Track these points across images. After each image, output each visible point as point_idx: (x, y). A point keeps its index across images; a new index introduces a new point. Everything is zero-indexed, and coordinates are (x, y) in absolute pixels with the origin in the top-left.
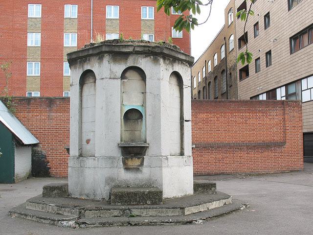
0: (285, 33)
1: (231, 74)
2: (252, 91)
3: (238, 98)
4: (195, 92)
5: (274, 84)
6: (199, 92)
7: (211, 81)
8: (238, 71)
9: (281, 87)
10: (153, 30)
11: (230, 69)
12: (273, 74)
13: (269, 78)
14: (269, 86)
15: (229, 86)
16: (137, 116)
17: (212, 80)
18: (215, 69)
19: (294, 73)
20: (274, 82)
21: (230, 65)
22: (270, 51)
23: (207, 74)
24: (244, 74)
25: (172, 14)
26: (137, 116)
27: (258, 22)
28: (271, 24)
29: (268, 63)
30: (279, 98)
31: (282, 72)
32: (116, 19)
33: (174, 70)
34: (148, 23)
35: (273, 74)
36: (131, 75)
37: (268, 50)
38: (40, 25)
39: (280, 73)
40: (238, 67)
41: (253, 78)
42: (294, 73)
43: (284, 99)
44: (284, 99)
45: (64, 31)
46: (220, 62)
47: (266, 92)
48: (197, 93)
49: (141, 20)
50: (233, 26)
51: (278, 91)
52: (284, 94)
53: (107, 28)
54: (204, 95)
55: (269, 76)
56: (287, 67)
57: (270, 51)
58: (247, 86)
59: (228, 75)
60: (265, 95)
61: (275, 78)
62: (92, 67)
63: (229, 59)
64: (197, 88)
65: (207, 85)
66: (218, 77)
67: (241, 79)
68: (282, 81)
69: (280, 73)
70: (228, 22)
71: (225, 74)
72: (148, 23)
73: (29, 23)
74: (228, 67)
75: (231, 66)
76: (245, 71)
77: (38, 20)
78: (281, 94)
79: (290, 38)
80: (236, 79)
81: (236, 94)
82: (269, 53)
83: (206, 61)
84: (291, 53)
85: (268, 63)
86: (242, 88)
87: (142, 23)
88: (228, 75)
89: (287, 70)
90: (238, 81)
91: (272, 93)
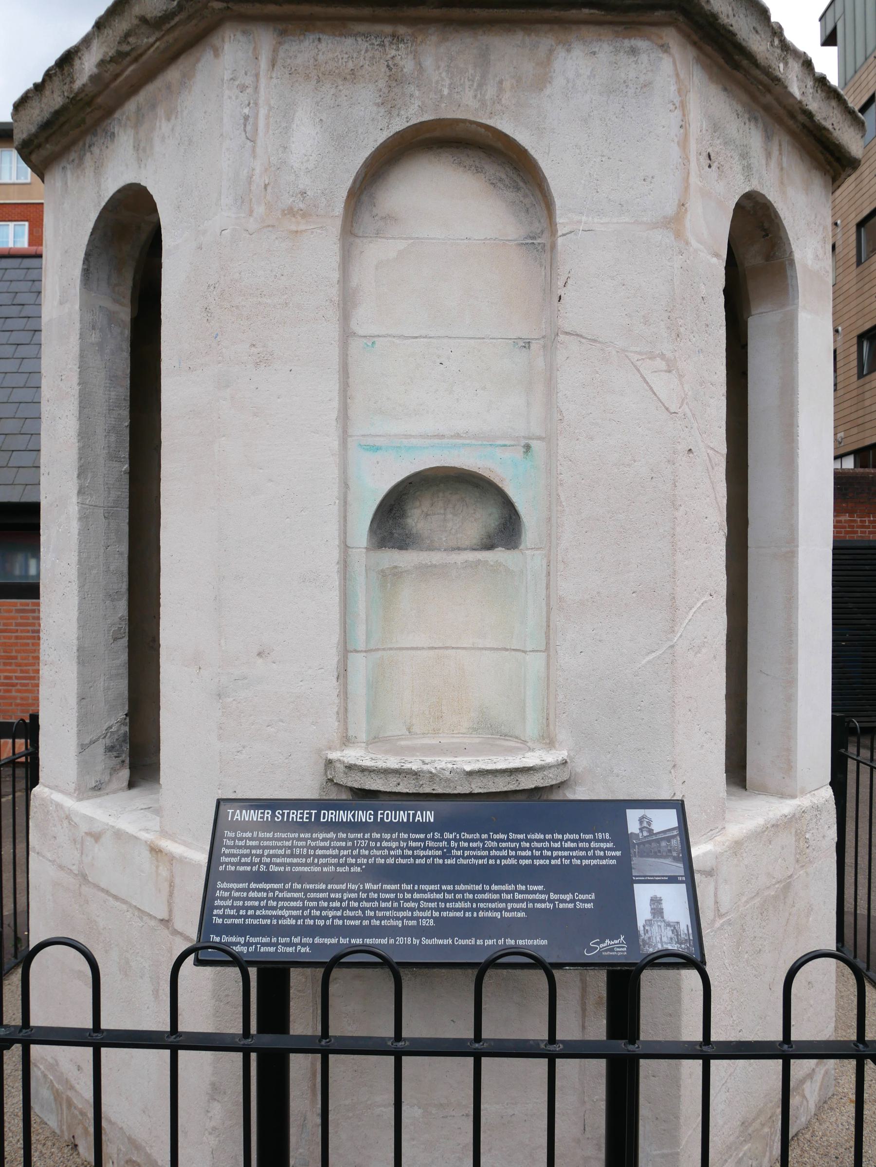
14: (868, 433)
16: (478, 520)
26: (478, 520)
55: (867, 403)
62: (141, 150)
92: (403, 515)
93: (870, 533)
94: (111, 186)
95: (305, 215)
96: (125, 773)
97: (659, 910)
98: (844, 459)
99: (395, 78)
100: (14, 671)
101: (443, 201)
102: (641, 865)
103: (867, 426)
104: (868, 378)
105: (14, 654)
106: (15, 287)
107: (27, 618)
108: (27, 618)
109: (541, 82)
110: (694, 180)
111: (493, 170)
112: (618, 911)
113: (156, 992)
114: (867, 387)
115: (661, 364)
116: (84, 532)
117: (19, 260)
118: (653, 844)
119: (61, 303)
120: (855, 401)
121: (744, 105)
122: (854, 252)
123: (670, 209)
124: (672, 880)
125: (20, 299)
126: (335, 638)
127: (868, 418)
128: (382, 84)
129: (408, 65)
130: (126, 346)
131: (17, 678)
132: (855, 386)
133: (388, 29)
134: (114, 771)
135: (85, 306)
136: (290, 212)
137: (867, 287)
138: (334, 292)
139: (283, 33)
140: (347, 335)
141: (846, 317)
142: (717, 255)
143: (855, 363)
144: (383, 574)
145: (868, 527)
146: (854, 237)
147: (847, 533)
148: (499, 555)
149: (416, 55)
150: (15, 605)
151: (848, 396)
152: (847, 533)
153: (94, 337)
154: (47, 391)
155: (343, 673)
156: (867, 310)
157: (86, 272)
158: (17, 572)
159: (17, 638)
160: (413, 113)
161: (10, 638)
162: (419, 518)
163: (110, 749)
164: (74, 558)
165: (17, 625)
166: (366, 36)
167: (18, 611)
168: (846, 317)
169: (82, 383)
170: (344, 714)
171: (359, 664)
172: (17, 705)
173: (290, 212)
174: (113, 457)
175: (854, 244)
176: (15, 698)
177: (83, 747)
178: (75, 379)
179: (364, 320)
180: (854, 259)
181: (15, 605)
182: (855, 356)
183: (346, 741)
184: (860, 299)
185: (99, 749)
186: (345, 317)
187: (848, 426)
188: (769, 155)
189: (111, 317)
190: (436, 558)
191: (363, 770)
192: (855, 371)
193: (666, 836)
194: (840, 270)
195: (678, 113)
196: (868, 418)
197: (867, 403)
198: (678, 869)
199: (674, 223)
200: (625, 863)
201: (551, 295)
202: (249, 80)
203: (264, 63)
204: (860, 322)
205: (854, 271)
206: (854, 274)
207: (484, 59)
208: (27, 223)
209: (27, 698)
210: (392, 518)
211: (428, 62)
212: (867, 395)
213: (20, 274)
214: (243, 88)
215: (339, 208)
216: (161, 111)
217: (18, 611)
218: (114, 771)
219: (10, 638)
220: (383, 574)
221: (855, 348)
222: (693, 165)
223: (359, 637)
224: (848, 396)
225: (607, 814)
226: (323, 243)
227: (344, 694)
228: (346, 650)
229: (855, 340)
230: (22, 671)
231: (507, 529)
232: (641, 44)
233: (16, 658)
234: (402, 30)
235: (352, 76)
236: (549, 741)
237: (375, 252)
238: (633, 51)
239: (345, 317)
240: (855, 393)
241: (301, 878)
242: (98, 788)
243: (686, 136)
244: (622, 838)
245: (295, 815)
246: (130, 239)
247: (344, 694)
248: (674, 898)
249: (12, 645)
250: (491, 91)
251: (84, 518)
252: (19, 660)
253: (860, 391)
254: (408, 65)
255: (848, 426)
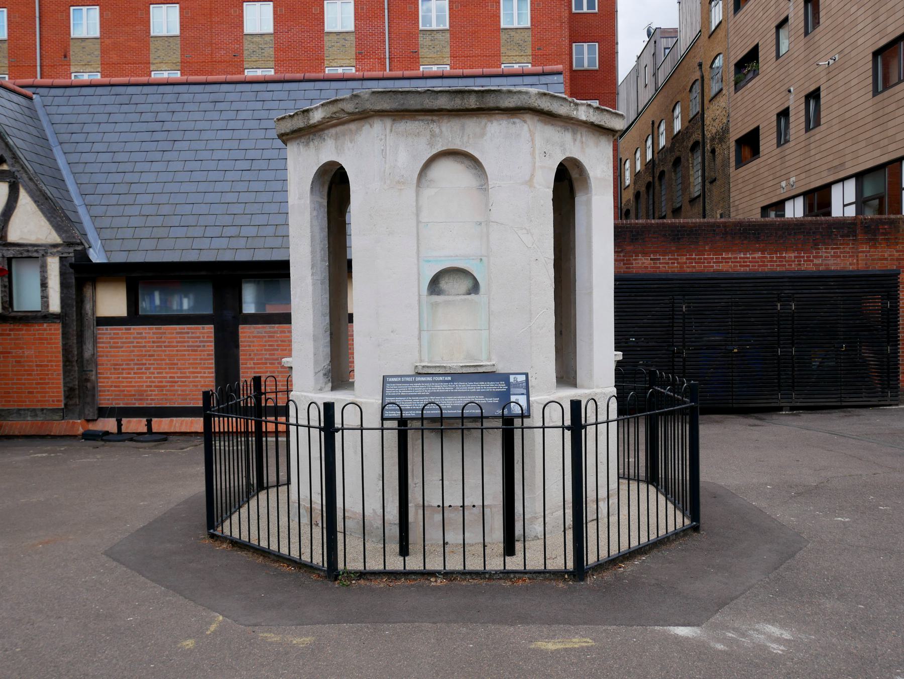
0: (860, 42)
1: (713, 151)
2: (766, 191)
3: (732, 215)
4: (628, 195)
5: (825, 174)
6: (637, 196)
7: (666, 169)
8: (733, 145)
9: (843, 180)
10: (529, 52)
11: (713, 139)
12: (823, 147)
13: (813, 159)
14: (813, 178)
15: (708, 181)
16: (465, 284)
17: (668, 167)
18: (676, 140)
19: (882, 143)
20: (825, 167)
21: (712, 128)
22: (818, 89)
23: (656, 152)
24: (746, 151)
25: (574, 11)
26: (465, 284)
27: (757, 46)
28: (821, 21)
29: (812, 122)
30: (837, 211)
31: (849, 143)
32: (443, 31)
33: (568, 155)
34: (517, 37)
35: (823, 147)
36: (448, 170)
37: (812, 88)
38: (271, 52)
39: (842, 146)
40: (731, 135)
41: (770, 161)
42: (882, 143)
43: (851, 212)
44: (851, 212)
45: (326, 62)
46: (687, 124)
47: (805, 194)
48: (632, 197)
49: (499, 29)
50: (721, 33)
51: (836, 191)
52: (851, 196)
53: (423, 52)
54: (647, 208)
55: (813, 152)
56: (861, 130)
57: (818, 89)
58: (755, 179)
59: (708, 155)
60: (800, 202)
61: (831, 158)
62: (339, 150)
63: (708, 116)
64: (632, 187)
65: (656, 179)
66: (682, 159)
67: (740, 163)
68: (848, 165)
69: (842, 146)
70: (710, 22)
71: (700, 159)
72: (517, 37)
73: (247, 46)
74: (708, 135)
75: (714, 131)
76: (750, 143)
77: (267, 39)
78: (843, 202)
79: (876, 54)
80: (726, 164)
81: (726, 197)
82: (814, 96)
83: (653, 123)
84: (876, 92)
85: (812, 122)
86: (740, 186)
87: (503, 36)
88: (708, 155)
89: (861, 137)
90: (732, 169)
91: (818, 200)
92: (439, 283)
93: (777, 265)
94: (325, 158)
95: (403, 183)
96: (330, 385)
97: (518, 400)
98: (846, 183)
99: (433, 135)
100: (176, 373)
101: (450, 174)
102: (513, 390)
103: (812, 172)
104: (812, 132)
105: (176, 361)
106: (156, 108)
107: (184, 338)
108: (184, 338)
109: (483, 135)
110: (537, 164)
111: (467, 162)
112: (507, 404)
113: (355, 452)
114: (812, 139)
115: (525, 231)
116: (314, 290)
117: (156, 87)
118: (517, 385)
119: (299, 199)
120: (803, 151)
121: (561, 127)
122: (802, 24)
123: (527, 178)
124: (523, 394)
125: (161, 117)
126: (417, 326)
127: (813, 165)
128: (428, 137)
129: (437, 130)
130: (326, 215)
131: (178, 377)
132: (803, 138)
133: (430, 118)
134: (326, 383)
135: (312, 201)
136: (398, 182)
137: (812, 55)
138: (414, 210)
139: (394, 120)
140: (418, 222)
141: (797, 79)
142: (549, 188)
143: (803, 119)
144: (432, 304)
145: (776, 261)
146: (802, 11)
147: (759, 266)
148: (473, 296)
149: (440, 127)
150: (176, 329)
151: (798, 147)
152: (759, 266)
153: (315, 213)
154: (292, 231)
155: (419, 338)
156: (811, 75)
157: (312, 188)
158: (175, 307)
159: (177, 351)
160: (439, 148)
161: (173, 351)
162: (444, 284)
163: (325, 375)
164: (310, 300)
165: (178, 342)
166: (422, 120)
167: (177, 333)
168: (797, 79)
169: (312, 232)
170: (420, 351)
171: (425, 335)
172: (179, 395)
173: (398, 182)
174: (322, 260)
175: (803, 18)
176: (177, 391)
177: (316, 373)
178: (309, 230)
179: (424, 217)
180: (803, 30)
181: (176, 329)
182: (803, 113)
183: (421, 361)
184: (807, 65)
185: (321, 374)
186: (418, 215)
187: (798, 172)
188: (575, 140)
189: (320, 204)
190: (450, 298)
191: (428, 367)
192: (803, 125)
193: (522, 382)
194: (792, 39)
195: (530, 144)
196: (813, 165)
197: (813, 152)
198: (525, 391)
199: (530, 182)
200: (508, 390)
201: (487, 207)
202: (383, 137)
203: (388, 130)
204: (807, 85)
205: (802, 40)
206: (802, 43)
207: (463, 128)
208: (98, 7)
209: (185, 391)
210: (435, 285)
211: (444, 129)
212: (813, 146)
213: (157, 98)
214: (381, 140)
215: (415, 181)
216: (347, 138)
217: (177, 333)
218: (326, 383)
219: (173, 351)
220: (432, 304)
221: (803, 106)
222: (537, 157)
223: (425, 327)
224: (798, 147)
225: (505, 377)
226: (410, 192)
227: (420, 345)
228: (420, 331)
229: (803, 100)
230: (181, 373)
231: (475, 288)
232: (517, 120)
233: (177, 364)
234: (435, 118)
235: (418, 135)
236: (489, 359)
237: (428, 193)
238: (514, 123)
239: (418, 215)
240: (803, 144)
241: (411, 396)
242: (321, 390)
243: (534, 150)
244: (508, 383)
245: (408, 379)
246: (335, 185)
247: (420, 345)
248: (522, 400)
249: (174, 355)
250: (465, 139)
251: (314, 284)
252: (179, 366)
253: (807, 142)
254: (437, 130)
255: (798, 172)
